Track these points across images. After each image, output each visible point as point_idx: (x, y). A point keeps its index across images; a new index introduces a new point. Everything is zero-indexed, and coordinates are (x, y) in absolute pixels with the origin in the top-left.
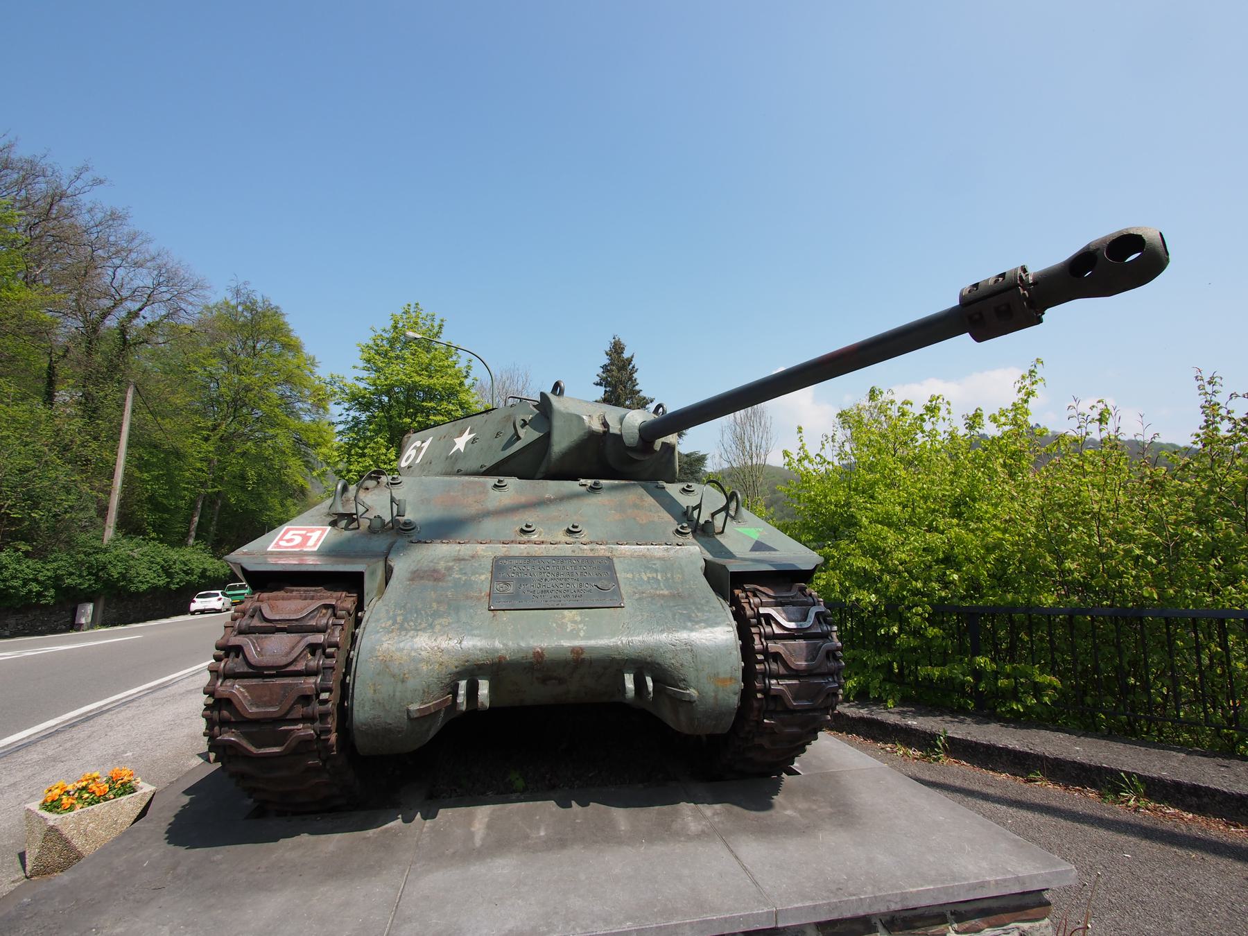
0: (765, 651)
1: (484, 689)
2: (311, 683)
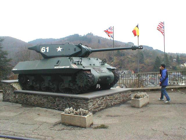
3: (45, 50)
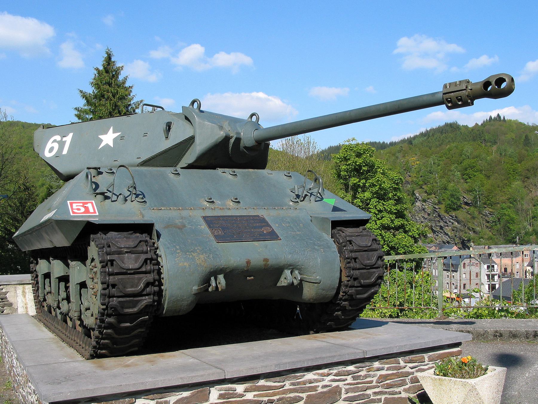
3: (56, 146)
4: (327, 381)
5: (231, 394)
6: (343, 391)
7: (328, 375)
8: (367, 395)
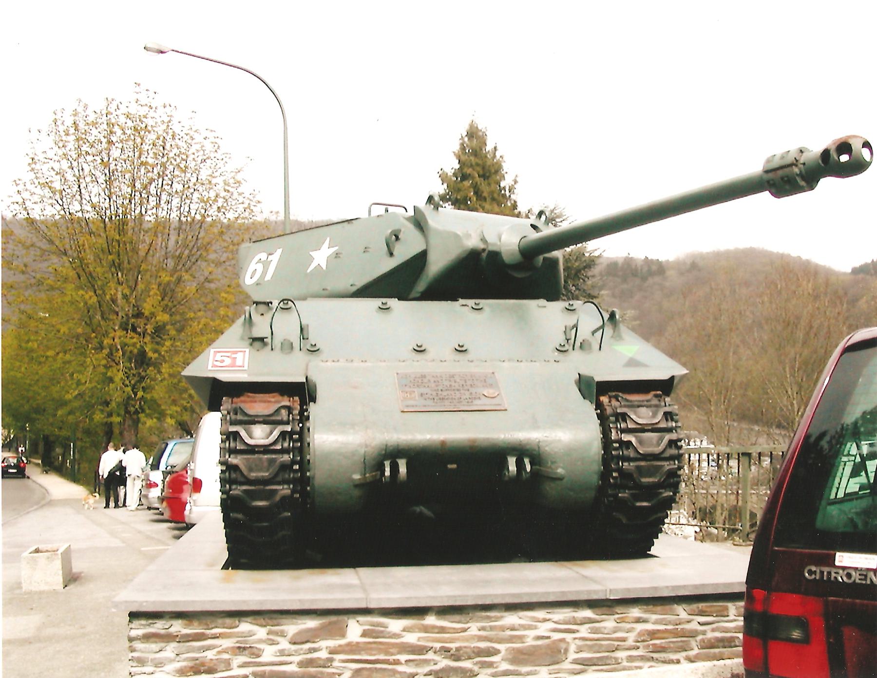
0: (620, 441)
1: (403, 469)
2: (286, 458)
3: (260, 268)
4: (543, 629)
5: (382, 632)
6: (573, 648)
7: (545, 620)
8: (616, 659)
